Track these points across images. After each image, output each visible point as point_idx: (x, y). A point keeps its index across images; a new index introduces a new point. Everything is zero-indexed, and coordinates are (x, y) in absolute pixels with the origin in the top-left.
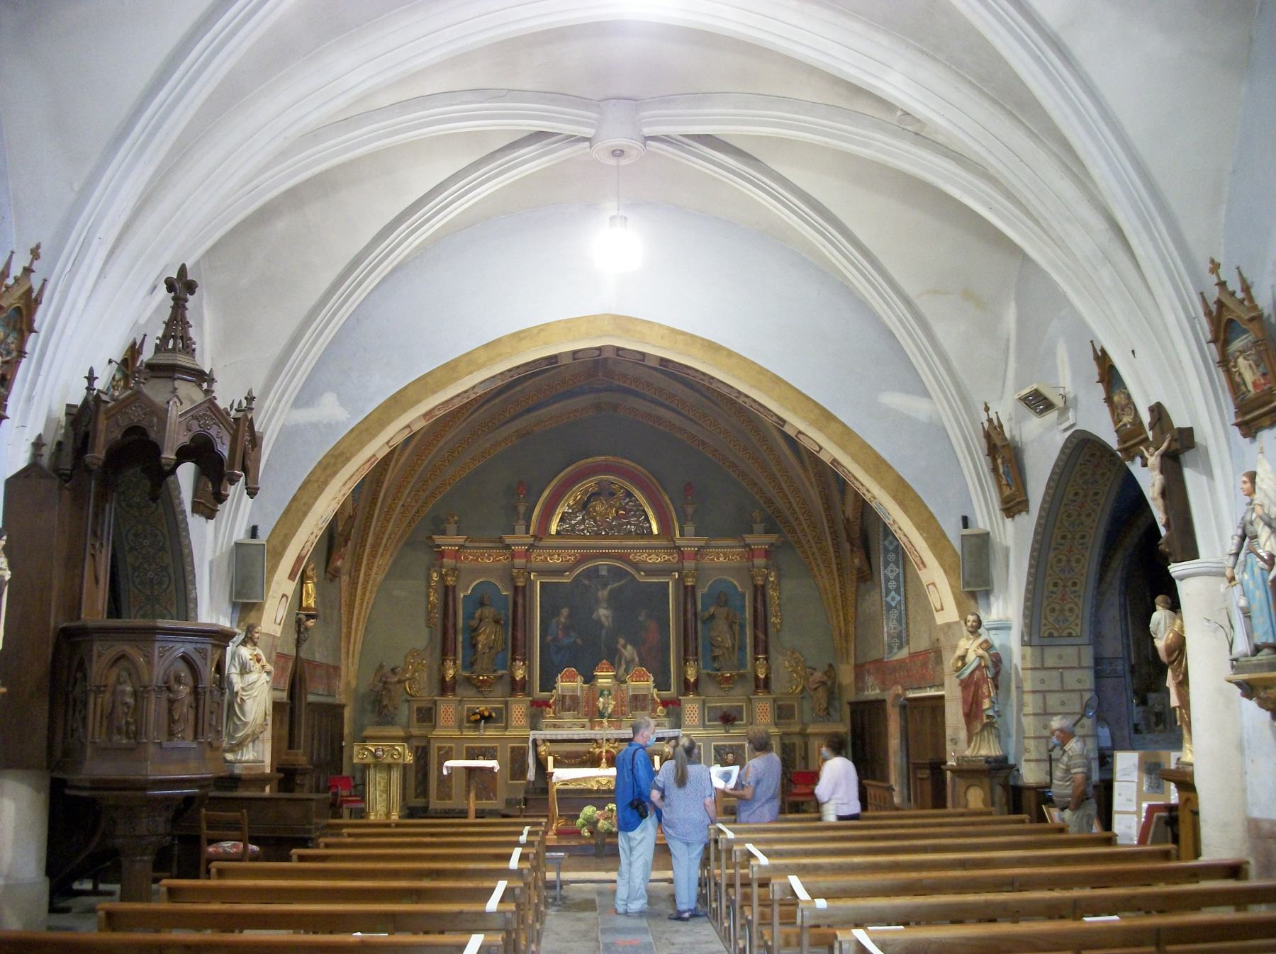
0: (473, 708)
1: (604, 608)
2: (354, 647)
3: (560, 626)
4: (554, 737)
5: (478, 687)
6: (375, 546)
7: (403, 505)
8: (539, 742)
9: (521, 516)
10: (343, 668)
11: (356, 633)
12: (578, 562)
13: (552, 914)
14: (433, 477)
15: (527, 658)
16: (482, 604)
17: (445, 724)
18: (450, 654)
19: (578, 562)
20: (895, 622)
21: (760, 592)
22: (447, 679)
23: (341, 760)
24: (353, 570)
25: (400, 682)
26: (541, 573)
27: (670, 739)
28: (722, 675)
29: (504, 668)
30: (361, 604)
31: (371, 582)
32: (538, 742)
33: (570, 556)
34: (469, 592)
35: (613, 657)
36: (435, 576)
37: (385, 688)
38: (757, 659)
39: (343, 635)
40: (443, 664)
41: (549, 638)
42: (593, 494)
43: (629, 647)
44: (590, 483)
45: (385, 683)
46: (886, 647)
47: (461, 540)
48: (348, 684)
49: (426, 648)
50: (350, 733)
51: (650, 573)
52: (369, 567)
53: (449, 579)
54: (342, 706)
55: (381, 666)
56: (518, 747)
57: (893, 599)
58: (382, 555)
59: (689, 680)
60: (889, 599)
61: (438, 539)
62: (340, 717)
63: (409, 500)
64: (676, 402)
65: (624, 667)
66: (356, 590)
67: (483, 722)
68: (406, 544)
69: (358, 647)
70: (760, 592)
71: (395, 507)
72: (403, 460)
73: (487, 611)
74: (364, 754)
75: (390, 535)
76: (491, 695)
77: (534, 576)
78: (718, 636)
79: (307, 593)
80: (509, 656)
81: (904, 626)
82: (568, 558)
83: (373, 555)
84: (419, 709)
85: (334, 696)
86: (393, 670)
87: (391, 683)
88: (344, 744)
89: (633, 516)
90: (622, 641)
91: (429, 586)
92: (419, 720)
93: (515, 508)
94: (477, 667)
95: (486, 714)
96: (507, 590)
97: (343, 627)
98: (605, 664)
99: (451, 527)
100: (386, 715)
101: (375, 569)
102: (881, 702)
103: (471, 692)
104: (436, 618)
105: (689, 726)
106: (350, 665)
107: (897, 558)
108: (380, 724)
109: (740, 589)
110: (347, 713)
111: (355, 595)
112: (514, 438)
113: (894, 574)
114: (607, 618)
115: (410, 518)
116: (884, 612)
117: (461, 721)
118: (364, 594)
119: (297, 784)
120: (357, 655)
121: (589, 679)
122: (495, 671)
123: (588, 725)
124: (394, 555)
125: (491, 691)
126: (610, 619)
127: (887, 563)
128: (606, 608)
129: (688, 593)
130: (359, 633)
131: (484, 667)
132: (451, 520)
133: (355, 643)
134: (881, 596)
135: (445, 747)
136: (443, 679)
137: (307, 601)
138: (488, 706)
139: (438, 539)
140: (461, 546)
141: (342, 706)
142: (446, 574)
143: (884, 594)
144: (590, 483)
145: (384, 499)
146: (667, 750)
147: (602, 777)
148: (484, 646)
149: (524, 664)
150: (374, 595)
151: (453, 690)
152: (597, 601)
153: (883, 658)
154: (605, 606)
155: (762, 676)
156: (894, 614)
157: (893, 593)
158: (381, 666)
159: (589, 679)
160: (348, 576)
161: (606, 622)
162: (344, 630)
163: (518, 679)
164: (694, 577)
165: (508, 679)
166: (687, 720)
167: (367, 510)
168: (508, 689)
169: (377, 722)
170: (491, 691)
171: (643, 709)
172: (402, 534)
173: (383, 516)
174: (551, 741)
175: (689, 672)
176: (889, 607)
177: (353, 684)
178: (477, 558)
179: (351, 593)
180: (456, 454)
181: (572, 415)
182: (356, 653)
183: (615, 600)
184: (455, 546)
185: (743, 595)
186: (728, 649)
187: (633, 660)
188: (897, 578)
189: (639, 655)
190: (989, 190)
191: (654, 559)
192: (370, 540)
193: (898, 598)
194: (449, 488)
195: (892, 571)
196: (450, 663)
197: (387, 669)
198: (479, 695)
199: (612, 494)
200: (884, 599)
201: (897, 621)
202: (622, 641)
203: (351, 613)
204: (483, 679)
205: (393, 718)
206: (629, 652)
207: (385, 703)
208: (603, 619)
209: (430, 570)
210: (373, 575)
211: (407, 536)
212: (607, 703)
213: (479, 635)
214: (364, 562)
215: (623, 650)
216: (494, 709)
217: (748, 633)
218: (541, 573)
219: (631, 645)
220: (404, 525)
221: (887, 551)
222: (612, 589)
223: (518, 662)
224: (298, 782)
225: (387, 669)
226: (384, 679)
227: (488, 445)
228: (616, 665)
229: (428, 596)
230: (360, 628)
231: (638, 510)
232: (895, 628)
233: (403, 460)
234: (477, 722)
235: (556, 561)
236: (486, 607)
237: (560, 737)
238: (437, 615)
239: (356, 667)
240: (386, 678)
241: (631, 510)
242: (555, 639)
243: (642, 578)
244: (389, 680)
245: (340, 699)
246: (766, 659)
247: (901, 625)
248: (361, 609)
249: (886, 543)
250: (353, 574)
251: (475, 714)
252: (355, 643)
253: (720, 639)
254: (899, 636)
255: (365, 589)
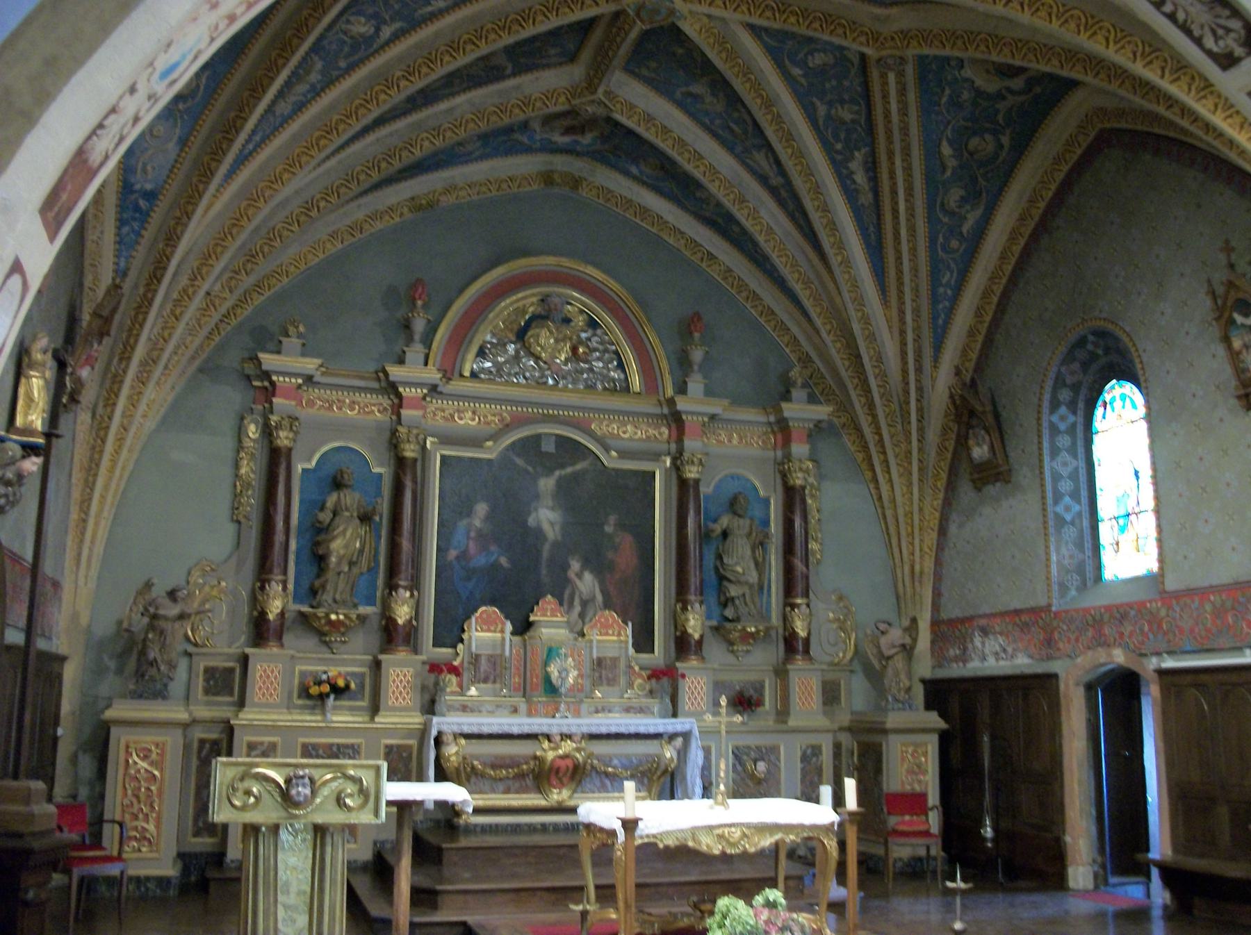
0: (317, 672)
1: (547, 508)
2: (91, 550)
3: (473, 534)
4: (475, 730)
5: (321, 634)
6: (150, 362)
7: (208, 294)
8: (448, 738)
9: (417, 337)
10: (67, 585)
11: (97, 524)
12: (507, 428)
13: (1108, 574)
14: (266, 249)
15: (415, 585)
16: (337, 484)
17: (264, 700)
18: (276, 570)
19: (507, 428)
20: (1071, 546)
21: (793, 497)
22: (271, 617)
23: (53, 764)
24: (101, 404)
25: (182, 617)
26: (446, 440)
27: (672, 737)
28: (744, 629)
29: (370, 601)
30: (112, 470)
31: (133, 430)
32: (445, 738)
33: (492, 415)
34: (314, 463)
35: (561, 590)
36: (253, 431)
37: (151, 627)
38: (793, 606)
39: (72, 524)
40: (262, 588)
41: (453, 554)
42: (535, 318)
43: (588, 577)
44: (527, 300)
45: (155, 617)
46: (1055, 587)
47: (310, 365)
48: (75, 616)
49: (229, 557)
50: (73, 713)
51: (623, 454)
52: (133, 403)
53: (282, 434)
54: (62, 659)
55: (148, 585)
56: (399, 746)
57: (1068, 509)
58: (158, 383)
59: (690, 635)
60: (1060, 509)
61: (268, 360)
62: (55, 681)
63: (218, 287)
64: (702, 169)
65: (577, 608)
66: (104, 441)
67: (332, 697)
68: (201, 370)
69: (99, 549)
70: (793, 497)
71: (194, 293)
72: (218, 206)
73: (350, 498)
74: (248, 793)
75: (178, 347)
76: (343, 648)
77: (432, 443)
78: (737, 564)
79: (30, 399)
80: (380, 582)
81: (1089, 553)
82: (490, 418)
83: (142, 380)
84: (210, 672)
85: (50, 638)
86: (172, 595)
87: (166, 618)
88: (60, 731)
89: (598, 359)
90: (575, 565)
91: (240, 447)
92: (207, 691)
93: (407, 326)
94: (327, 597)
95: (341, 683)
96: (381, 465)
97: (72, 509)
98: (549, 603)
99: (292, 342)
100: (153, 679)
101: (142, 407)
102: (1047, 682)
103: (311, 642)
104: (251, 505)
105: (394, 709)
106: (81, 581)
107: (1074, 443)
108: (140, 697)
109: (762, 493)
110: (70, 673)
111: (101, 452)
112: (406, 210)
113: (1070, 469)
114: (552, 524)
115: (213, 325)
116: (1051, 530)
117: (290, 697)
118: (117, 452)
119: (26, 904)
120: (96, 565)
121: (524, 627)
122: (355, 606)
123: (523, 707)
124: (178, 389)
125: (344, 642)
126: (557, 528)
127: (1055, 453)
128: (553, 509)
129: (685, 489)
130: (103, 523)
131: (338, 597)
132: (292, 330)
133: (92, 542)
134: (1044, 498)
135: (262, 743)
136: (263, 614)
137: (26, 415)
138: (343, 669)
139: (268, 360)
140: (309, 379)
141: (62, 659)
142: (279, 426)
143: (1050, 501)
144: (527, 300)
145: (175, 274)
146: (668, 755)
147: (731, 825)
148: (340, 559)
149: (412, 595)
150: (135, 456)
151: (280, 637)
152: (537, 497)
153: (1050, 605)
154: (550, 503)
155: (802, 633)
156: (1070, 533)
157: (1067, 499)
158: (148, 585)
159: (524, 627)
160: (90, 415)
161: (551, 533)
162: (74, 516)
163: (400, 622)
164: (701, 463)
165: (375, 622)
166: (686, 702)
167: (141, 290)
168: (375, 639)
169: (135, 692)
170: (344, 642)
171: (611, 682)
172: (196, 352)
173: (169, 306)
174: (468, 736)
175: (692, 622)
176: (1060, 521)
177: (84, 620)
178: (331, 406)
179: (93, 448)
180: (314, 213)
181: (504, 186)
182: (94, 560)
183: (566, 493)
184: (296, 375)
185: (766, 502)
186: (751, 586)
187: (593, 599)
188: (1074, 476)
189: (604, 592)
190: (514, 298)
191: (632, 433)
192: (140, 352)
193: (1077, 508)
194: (285, 280)
195: (1065, 464)
196: (275, 588)
197: (159, 591)
198: (324, 649)
199: (567, 321)
200: (1050, 509)
201: (1075, 544)
202: (575, 565)
203: (89, 485)
204: (338, 621)
205: (166, 686)
206: (587, 584)
207: (152, 655)
208: (546, 527)
209: (242, 418)
210: (138, 418)
211: (204, 356)
212: (565, 671)
213: (334, 538)
214: (125, 391)
215: (578, 582)
216: (353, 674)
217: (773, 563)
218: (446, 440)
219: (591, 572)
220: (204, 333)
221: (1054, 430)
222: (560, 477)
223: (401, 591)
224: (31, 895)
225: (159, 591)
226: (152, 610)
227: (360, 215)
228: (565, 604)
229: (237, 466)
230: (105, 514)
231: (606, 351)
232: (1071, 557)
233: (218, 206)
234: (322, 697)
235: (467, 422)
236: (347, 491)
237: (486, 730)
238: (252, 502)
239: (92, 585)
240: (157, 608)
241: (596, 350)
242: (463, 556)
243: (611, 460)
244: (161, 612)
245: (59, 645)
246: (808, 605)
247: (1084, 553)
248: (110, 478)
249: (1055, 418)
250: (100, 410)
251: (319, 683)
252: (92, 542)
253: (739, 569)
254: (1080, 569)
255: (120, 440)
